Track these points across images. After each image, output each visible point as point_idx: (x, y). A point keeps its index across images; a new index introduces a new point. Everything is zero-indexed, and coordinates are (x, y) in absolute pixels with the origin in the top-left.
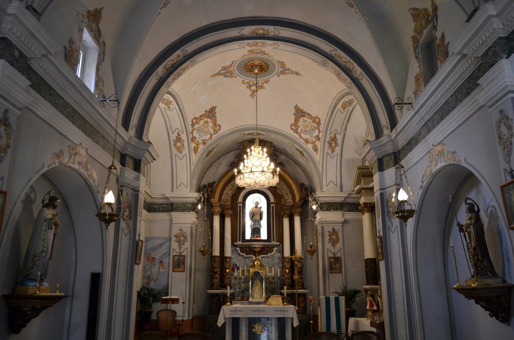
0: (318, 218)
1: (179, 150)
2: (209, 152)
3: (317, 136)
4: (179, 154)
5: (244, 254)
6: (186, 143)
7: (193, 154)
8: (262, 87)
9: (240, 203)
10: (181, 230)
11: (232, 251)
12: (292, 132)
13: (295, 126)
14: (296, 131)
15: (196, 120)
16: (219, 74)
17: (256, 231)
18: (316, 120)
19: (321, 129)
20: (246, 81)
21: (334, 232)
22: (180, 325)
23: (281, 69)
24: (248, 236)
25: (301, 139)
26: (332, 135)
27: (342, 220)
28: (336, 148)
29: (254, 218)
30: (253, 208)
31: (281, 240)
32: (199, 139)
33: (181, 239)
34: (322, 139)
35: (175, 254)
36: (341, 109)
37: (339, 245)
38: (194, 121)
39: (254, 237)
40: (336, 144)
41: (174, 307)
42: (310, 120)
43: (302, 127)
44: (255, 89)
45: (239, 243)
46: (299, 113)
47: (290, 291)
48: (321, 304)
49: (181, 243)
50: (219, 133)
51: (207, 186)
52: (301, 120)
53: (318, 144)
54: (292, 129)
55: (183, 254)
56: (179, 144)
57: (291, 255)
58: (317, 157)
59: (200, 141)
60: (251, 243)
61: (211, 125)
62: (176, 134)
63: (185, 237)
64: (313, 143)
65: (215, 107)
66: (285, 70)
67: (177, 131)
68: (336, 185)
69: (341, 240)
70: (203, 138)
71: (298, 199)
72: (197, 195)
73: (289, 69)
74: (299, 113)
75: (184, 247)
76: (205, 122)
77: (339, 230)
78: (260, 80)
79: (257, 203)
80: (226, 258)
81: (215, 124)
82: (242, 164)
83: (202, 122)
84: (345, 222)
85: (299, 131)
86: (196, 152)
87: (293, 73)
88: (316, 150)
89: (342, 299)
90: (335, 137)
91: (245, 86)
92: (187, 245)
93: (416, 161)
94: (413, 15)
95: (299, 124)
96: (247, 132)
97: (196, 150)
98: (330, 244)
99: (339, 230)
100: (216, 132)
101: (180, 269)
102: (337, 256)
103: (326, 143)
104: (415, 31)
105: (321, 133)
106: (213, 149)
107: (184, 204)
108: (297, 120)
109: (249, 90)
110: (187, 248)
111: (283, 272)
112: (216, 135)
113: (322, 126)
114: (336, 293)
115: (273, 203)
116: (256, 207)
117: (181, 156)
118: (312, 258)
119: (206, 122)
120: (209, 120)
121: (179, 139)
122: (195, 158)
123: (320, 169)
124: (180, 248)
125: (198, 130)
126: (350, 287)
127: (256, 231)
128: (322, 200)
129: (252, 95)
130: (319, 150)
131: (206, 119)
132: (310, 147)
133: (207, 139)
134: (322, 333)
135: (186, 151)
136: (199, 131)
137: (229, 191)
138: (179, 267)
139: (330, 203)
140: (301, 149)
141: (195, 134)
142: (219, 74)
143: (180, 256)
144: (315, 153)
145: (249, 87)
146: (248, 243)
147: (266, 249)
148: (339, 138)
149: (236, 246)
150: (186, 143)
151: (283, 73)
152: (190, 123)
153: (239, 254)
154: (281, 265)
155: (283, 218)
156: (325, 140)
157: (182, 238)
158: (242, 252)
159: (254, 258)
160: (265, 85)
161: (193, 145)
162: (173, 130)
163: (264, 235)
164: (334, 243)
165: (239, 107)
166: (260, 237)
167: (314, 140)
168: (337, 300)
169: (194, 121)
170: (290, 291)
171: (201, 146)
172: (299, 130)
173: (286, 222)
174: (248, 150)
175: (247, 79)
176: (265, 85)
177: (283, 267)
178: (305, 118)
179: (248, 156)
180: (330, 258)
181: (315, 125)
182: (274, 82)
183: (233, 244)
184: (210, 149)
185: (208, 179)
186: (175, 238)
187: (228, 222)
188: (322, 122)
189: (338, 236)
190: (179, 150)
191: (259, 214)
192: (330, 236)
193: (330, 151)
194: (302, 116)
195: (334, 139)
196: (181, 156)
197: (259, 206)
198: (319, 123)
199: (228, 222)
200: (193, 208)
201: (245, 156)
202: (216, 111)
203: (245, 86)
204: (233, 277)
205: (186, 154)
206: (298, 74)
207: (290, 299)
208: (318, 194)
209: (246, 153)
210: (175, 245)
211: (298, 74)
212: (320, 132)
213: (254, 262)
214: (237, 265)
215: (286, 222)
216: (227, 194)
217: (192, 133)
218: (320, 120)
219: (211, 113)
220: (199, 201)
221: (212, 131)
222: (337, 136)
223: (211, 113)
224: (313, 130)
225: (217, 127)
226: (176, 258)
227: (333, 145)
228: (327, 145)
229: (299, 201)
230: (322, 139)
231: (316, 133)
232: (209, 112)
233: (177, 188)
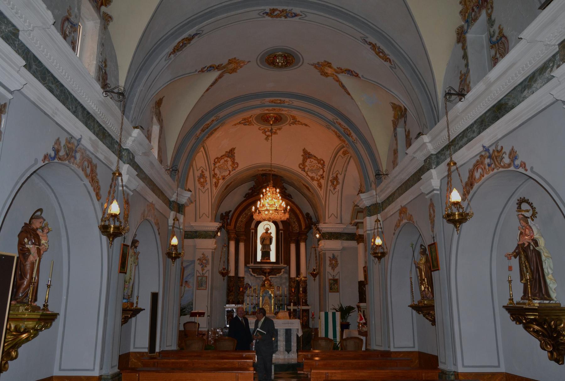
0: (320, 246)
1: (202, 185)
2: (228, 186)
3: (322, 175)
4: (202, 188)
5: (256, 275)
6: (208, 179)
7: (214, 188)
8: (275, 133)
9: (252, 229)
10: (203, 254)
11: (245, 272)
12: (300, 170)
13: (303, 166)
14: (303, 170)
15: (218, 159)
16: (240, 123)
17: (266, 254)
18: (321, 162)
19: (325, 170)
20: (262, 128)
21: (334, 258)
22: (204, 335)
23: (292, 121)
24: (259, 259)
25: (308, 177)
26: (335, 175)
27: (341, 248)
28: (338, 186)
29: (264, 243)
30: (263, 234)
31: (288, 262)
32: (219, 175)
33: (203, 262)
34: (326, 178)
35: (198, 275)
36: (342, 155)
37: (337, 270)
38: (216, 160)
39: (264, 259)
40: (338, 183)
41: (197, 319)
42: (316, 162)
43: (308, 167)
44: (269, 135)
45: (251, 265)
46: (307, 155)
47: (296, 308)
48: (321, 318)
49: (203, 265)
50: (237, 170)
51: (224, 214)
52: (308, 160)
53: (322, 181)
54: (300, 168)
55: (205, 275)
56: (202, 180)
57: (297, 277)
58: (321, 193)
59: (220, 177)
60: (262, 265)
61: (230, 163)
62: (200, 172)
63: (207, 261)
64: (318, 180)
65: (234, 149)
66: (295, 121)
67: (202, 169)
68: (337, 218)
69: (339, 265)
70: (223, 174)
71: (303, 227)
72: (217, 225)
73: (299, 121)
74: (307, 155)
75: (206, 269)
76: (225, 161)
77: (338, 256)
78: (275, 128)
79: (267, 229)
80: (239, 278)
81: (233, 163)
82: (259, 202)
83: (222, 161)
84: (344, 249)
85: (306, 169)
86: (216, 186)
87: (302, 124)
88: (320, 186)
89: (338, 315)
90: (337, 176)
91: (261, 132)
92: (209, 267)
93: (392, 213)
94: (393, 107)
95: (307, 164)
96: (261, 169)
97: (216, 185)
98: (330, 268)
99: (338, 256)
100: (234, 169)
101: (203, 288)
102: (336, 278)
103: (329, 182)
104: (394, 117)
105: (325, 173)
106: (231, 183)
107: (206, 232)
108: (304, 161)
109: (264, 135)
110: (209, 270)
111: (290, 290)
112: (234, 171)
113: (326, 167)
114: (334, 309)
115: (281, 230)
116: (267, 232)
117: (204, 190)
118: (314, 280)
119: (227, 161)
120: (229, 159)
121: (202, 176)
122: (215, 191)
123: (323, 203)
124: (203, 270)
125: (219, 168)
126: (344, 306)
127: (266, 254)
128: (324, 230)
129: (267, 139)
130: (323, 187)
131: (226, 159)
132: (315, 183)
133: (226, 175)
134: (322, 338)
135: (208, 186)
136: (220, 168)
137: (243, 219)
138: (202, 286)
139: (331, 233)
140: (307, 185)
141: (217, 171)
142: (240, 123)
143: (203, 276)
144: (319, 189)
145: (265, 132)
146: (259, 265)
147: (274, 271)
148: (340, 177)
149: (249, 268)
150: (208, 179)
151: (294, 123)
152: (213, 162)
153: (251, 275)
154: (287, 284)
155: (290, 243)
156: (328, 179)
157: (204, 261)
158: (254, 273)
159: (265, 278)
160: (278, 131)
161: (214, 180)
162: (198, 168)
163: (273, 258)
164: (333, 267)
165: (254, 149)
166: (269, 259)
167: (319, 178)
168: (334, 314)
169: (216, 160)
170: (296, 308)
171: (221, 181)
172: (306, 169)
173: (293, 247)
174: (264, 191)
175: (263, 127)
176: (278, 131)
177: (290, 287)
178: (312, 160)
179: (263, 196)
180: (330, 279)
181: (320, 165)
182: (286, 132)
183: (245, 265)
184: (228, 183)
185: (224, 209)
186: (199, 261)
187: (242, 246)
188: (326, 164)
189: (337, 261)
190: (202, 185)
191: (269, 239)
192: (330, 261)
193: (332, 188)
194: (309, 158)
195: (336, 178)
196: (204, 190)
197: (269, 232)
198: (323, 165)
199: (242, 246)
200: (213, 235)
201: (261, 196)
202: (235, 151)
203: (261, 132)
204: (245, 295)
205: (208, 189)
206: (306, 125)
207: (293, 315)
208: (321, 226)
209: (263, 193)
210: (198, 267)
211: (306, 125)
212: (324, 172)
213: (264, 281)
214: (249, 285)
215: (293, 247)
216: (242, 221)
217: (214, 170)
218: (324, 162)
219: (231, 153)
220: (219, 229)
221: (230, 168)
222: (339, 176)
223: (231, 153)
224: (318, 170)
225: (235, 164)
226: (200, 278)
227: (335, 183)
228: (330, 183)
229: (305, 229)
230: (326, 178)
231: (321, 172)
232: (229, 152)
233: (200, 218)
